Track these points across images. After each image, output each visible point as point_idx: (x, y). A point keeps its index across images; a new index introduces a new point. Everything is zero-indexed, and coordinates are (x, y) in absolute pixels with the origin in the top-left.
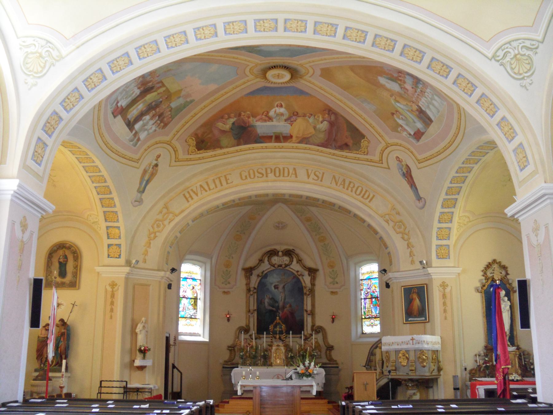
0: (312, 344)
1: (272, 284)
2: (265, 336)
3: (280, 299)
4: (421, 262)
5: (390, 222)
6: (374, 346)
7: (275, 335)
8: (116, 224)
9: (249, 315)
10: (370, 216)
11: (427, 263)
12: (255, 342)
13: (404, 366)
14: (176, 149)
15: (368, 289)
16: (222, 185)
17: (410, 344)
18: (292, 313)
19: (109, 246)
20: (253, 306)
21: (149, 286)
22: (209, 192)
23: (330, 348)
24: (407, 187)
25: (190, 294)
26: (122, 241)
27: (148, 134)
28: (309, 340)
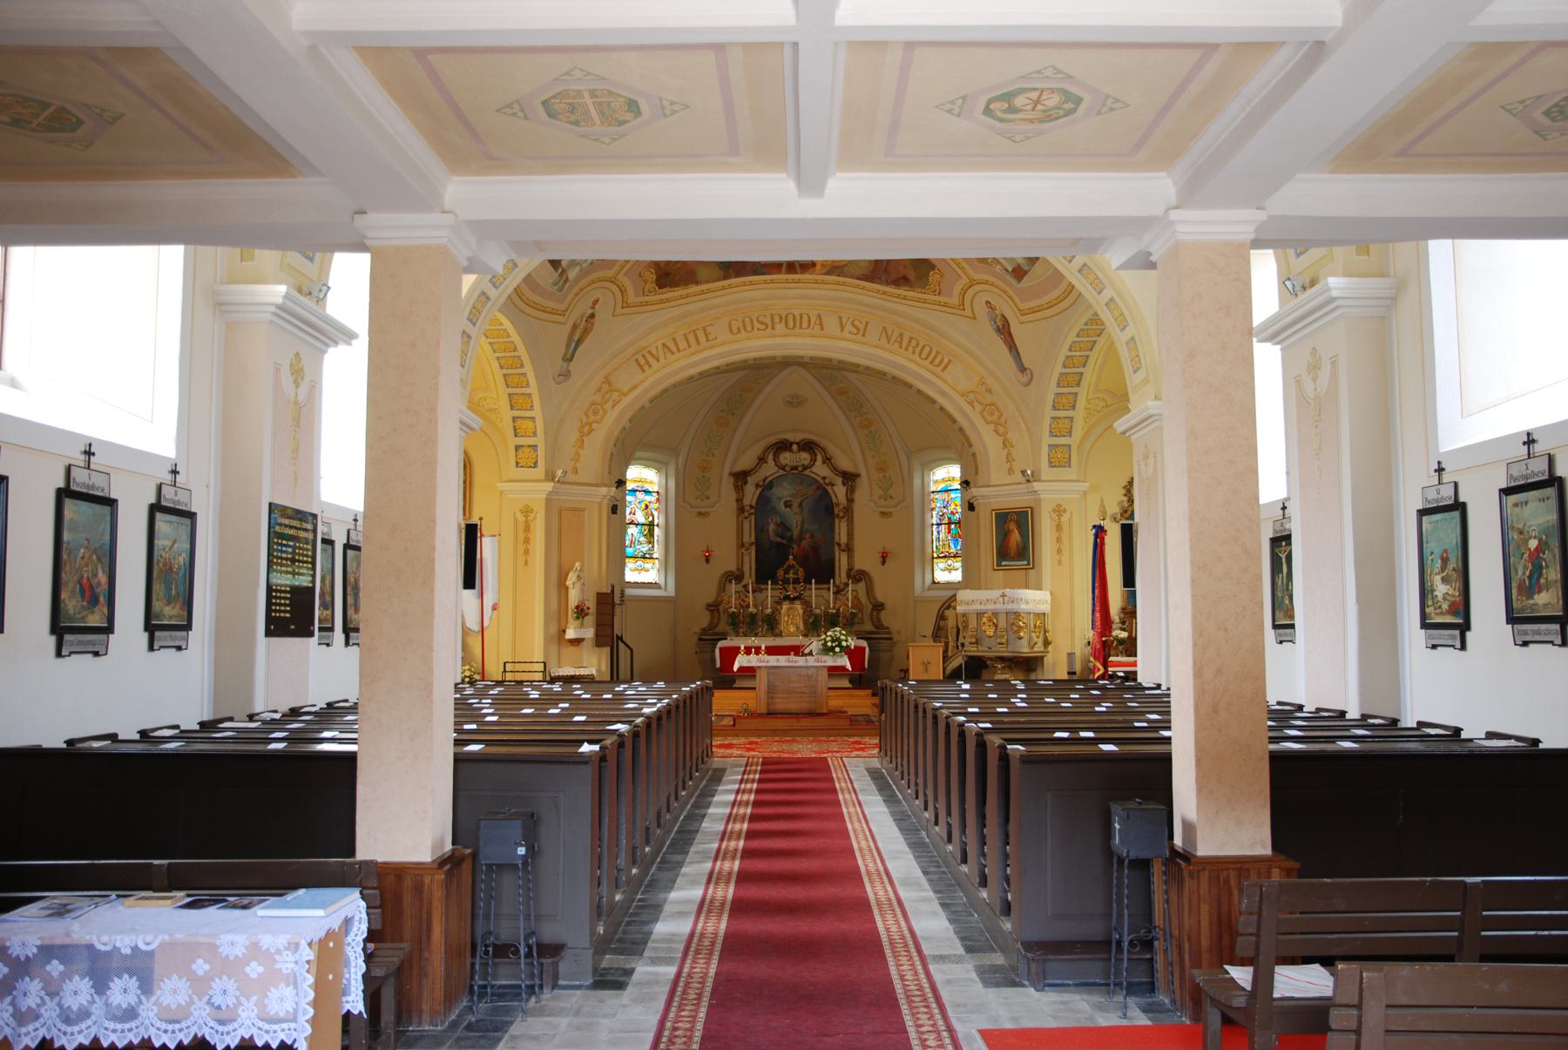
0: (848, 601)
1: (780, 499)
2: (769, 587)
3: (795, 525)
4: (1023, 472)
5: (976, 404)
6: (945, 606)
7: (786, 586)
8: (528, 414)
9: (742, 553)
10: (943, 393)
11: (1033, 473)
12: (754, 597)
13: (990, 637)
14: (623, 289)
15: (944, 507)
16: (698, 343)
17: (1000, 603)
18: (815, 549)
19: (517, 448)
20: (749, 537)
21: (583, 510)
22: (677, 356)
23: (879, 607)
24: (1005, 349)
25: (640, 518)
26: (539, 441)
27: (581, 270)
28: (843, 593)
